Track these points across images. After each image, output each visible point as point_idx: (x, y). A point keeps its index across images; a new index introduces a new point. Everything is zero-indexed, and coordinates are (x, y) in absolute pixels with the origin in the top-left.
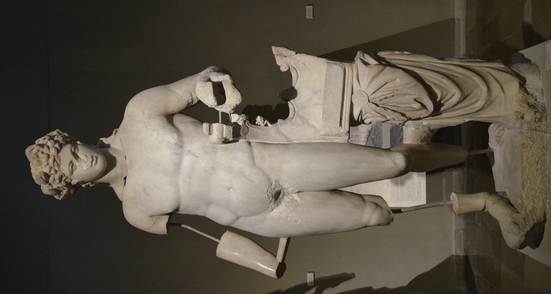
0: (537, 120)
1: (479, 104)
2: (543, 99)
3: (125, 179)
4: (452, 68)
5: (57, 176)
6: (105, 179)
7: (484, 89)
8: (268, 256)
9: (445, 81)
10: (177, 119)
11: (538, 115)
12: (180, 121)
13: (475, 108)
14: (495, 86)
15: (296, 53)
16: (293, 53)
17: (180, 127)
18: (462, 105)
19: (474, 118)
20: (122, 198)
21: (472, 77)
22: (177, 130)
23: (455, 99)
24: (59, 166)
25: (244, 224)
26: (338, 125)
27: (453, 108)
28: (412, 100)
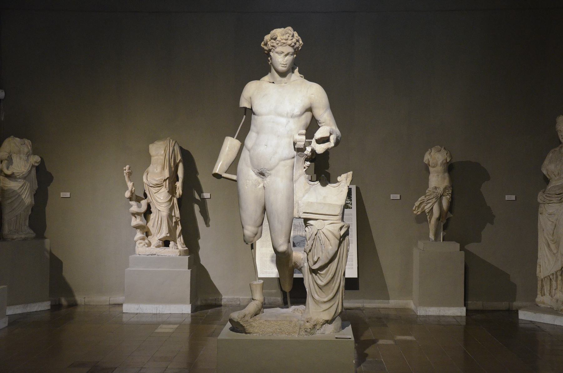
0: (306, 329)
1: (316, 297)
3: (273, 83)
6: (273, 70)
8: (226, 168)
9: (330, 276)
11: (309, 330)
14: (327, 306)
17: (304, 116)
18: (315, 284)
24: (281, 45)
25: (245, 154)
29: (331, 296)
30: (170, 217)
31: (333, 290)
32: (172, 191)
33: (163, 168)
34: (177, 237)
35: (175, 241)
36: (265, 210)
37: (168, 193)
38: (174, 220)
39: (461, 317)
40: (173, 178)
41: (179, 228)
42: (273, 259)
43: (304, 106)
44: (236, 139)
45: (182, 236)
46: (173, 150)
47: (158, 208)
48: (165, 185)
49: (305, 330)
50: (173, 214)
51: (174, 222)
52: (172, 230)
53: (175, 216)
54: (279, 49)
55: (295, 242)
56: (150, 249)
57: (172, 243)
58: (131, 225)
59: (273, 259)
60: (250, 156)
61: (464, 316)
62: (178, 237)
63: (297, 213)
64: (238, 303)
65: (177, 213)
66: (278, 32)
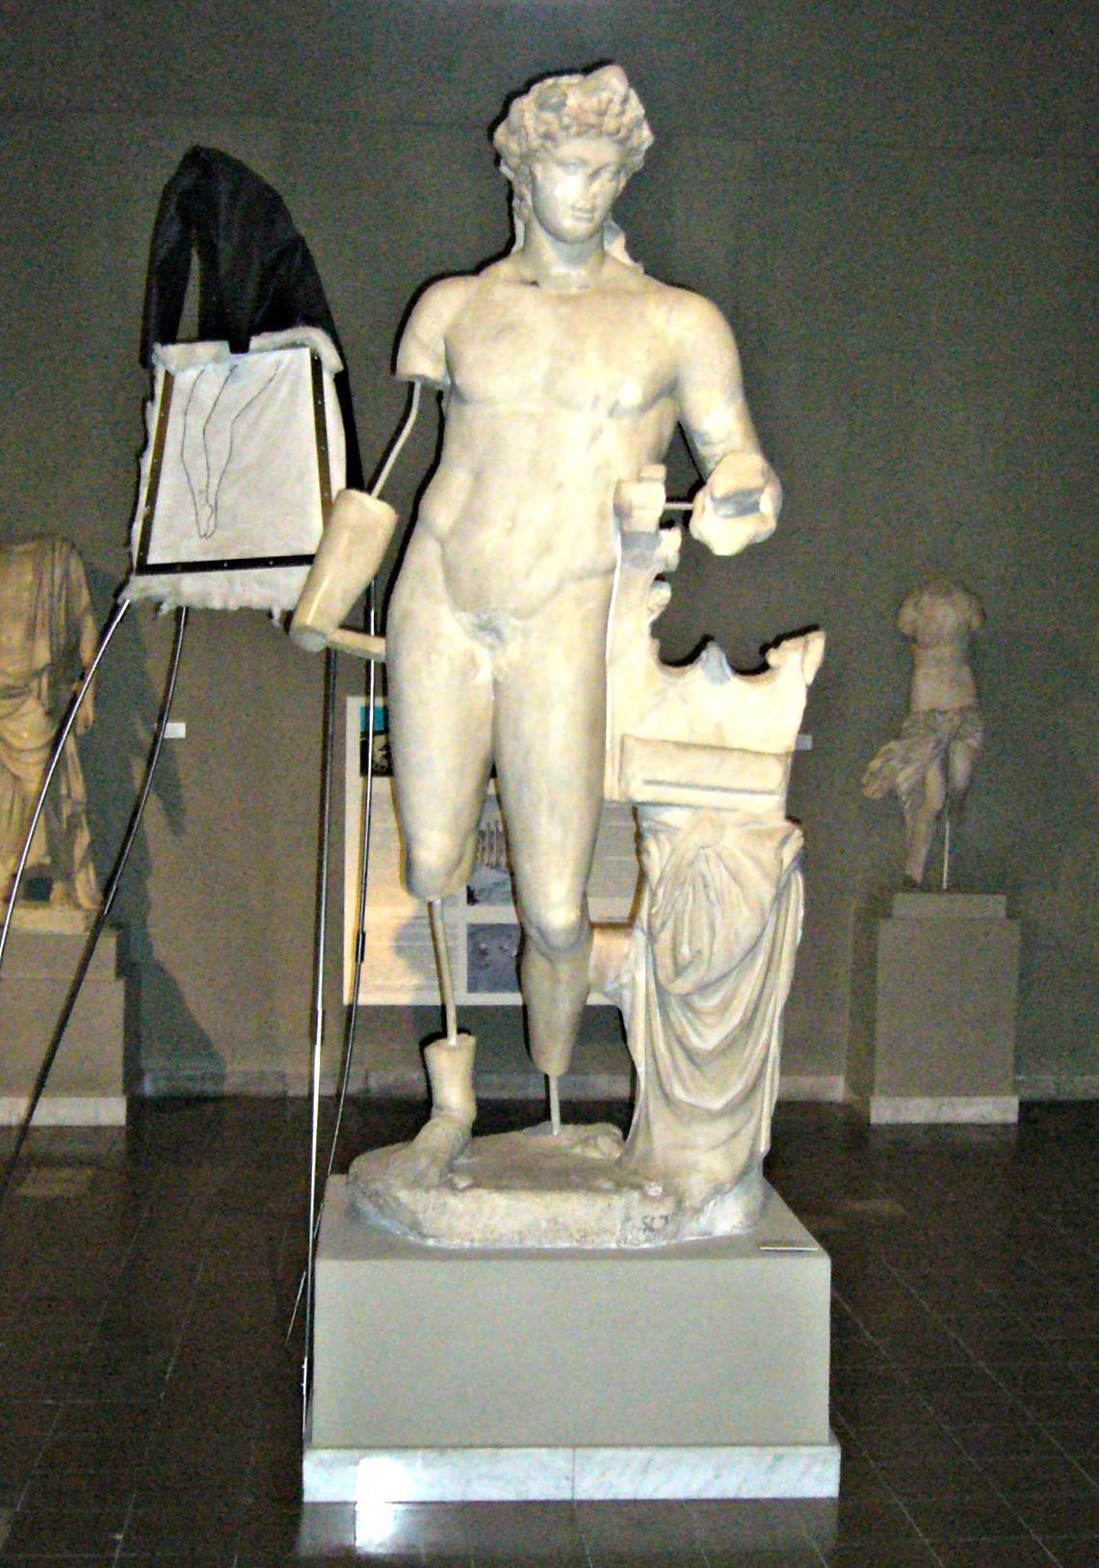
0: (648, 1221)
1: (679, 1092)
2: (692, 1234)
3: (534, 283)
4: (764, 1036)
5: (555, 127)
6: (541, 238)
7: (718, 1104)
8: (341, 609)
9: (735, 1018)
10: (665, 406)
11: (658, 1224)
12: (664, 411)
13: (671, 1086)
14: (723, 1128)
15: (240, 347)
16: (810, 678)
17: (653, 414)
18: (680, 1054)
19: (646, 1088)
20: (717, 463)
21: (745, 1076)
22: (646, 407)
23: (695, 1041)
24: (579, 135)
25: (423, 554)
26: (649, 777)
27: (673, 1038)
28: (697, 946)
29: (736, 1088)
30: (54, 800)
31: (745, 1067)
32: (60, 715)
33: (31, 634)
34: (77, 867)
35: (69, 877)
36: (493, 773)
37: (46, 719)
38: (66, 811)
39: (1005, 1126)
40: (67, 665)
41: (84, 839)
42: (401, 943)
43: (656, 373)
44: (381, 497)
45: (91, 866)
46: (66, 575)
47: (13, 769)
48: (35, 693)
49: (645, 1224)
50: (64, 791)
51: (65, 816)
52: (59, 844)
53: (69, 796)
54: (573, 148)
55: (476, 887)
56: (108, 917)
57: (58, 888)
58: (722, 646)
59: (401, 943)
60: (443, 558)
61: (1014, 1124)
62: (79, 871)
63: (617, 786)
64: (279, 1088)
65: (76, 786)
66: (575, 93)
